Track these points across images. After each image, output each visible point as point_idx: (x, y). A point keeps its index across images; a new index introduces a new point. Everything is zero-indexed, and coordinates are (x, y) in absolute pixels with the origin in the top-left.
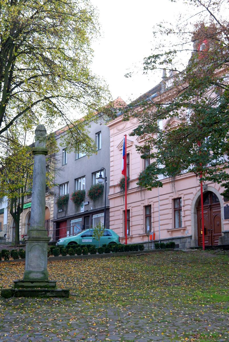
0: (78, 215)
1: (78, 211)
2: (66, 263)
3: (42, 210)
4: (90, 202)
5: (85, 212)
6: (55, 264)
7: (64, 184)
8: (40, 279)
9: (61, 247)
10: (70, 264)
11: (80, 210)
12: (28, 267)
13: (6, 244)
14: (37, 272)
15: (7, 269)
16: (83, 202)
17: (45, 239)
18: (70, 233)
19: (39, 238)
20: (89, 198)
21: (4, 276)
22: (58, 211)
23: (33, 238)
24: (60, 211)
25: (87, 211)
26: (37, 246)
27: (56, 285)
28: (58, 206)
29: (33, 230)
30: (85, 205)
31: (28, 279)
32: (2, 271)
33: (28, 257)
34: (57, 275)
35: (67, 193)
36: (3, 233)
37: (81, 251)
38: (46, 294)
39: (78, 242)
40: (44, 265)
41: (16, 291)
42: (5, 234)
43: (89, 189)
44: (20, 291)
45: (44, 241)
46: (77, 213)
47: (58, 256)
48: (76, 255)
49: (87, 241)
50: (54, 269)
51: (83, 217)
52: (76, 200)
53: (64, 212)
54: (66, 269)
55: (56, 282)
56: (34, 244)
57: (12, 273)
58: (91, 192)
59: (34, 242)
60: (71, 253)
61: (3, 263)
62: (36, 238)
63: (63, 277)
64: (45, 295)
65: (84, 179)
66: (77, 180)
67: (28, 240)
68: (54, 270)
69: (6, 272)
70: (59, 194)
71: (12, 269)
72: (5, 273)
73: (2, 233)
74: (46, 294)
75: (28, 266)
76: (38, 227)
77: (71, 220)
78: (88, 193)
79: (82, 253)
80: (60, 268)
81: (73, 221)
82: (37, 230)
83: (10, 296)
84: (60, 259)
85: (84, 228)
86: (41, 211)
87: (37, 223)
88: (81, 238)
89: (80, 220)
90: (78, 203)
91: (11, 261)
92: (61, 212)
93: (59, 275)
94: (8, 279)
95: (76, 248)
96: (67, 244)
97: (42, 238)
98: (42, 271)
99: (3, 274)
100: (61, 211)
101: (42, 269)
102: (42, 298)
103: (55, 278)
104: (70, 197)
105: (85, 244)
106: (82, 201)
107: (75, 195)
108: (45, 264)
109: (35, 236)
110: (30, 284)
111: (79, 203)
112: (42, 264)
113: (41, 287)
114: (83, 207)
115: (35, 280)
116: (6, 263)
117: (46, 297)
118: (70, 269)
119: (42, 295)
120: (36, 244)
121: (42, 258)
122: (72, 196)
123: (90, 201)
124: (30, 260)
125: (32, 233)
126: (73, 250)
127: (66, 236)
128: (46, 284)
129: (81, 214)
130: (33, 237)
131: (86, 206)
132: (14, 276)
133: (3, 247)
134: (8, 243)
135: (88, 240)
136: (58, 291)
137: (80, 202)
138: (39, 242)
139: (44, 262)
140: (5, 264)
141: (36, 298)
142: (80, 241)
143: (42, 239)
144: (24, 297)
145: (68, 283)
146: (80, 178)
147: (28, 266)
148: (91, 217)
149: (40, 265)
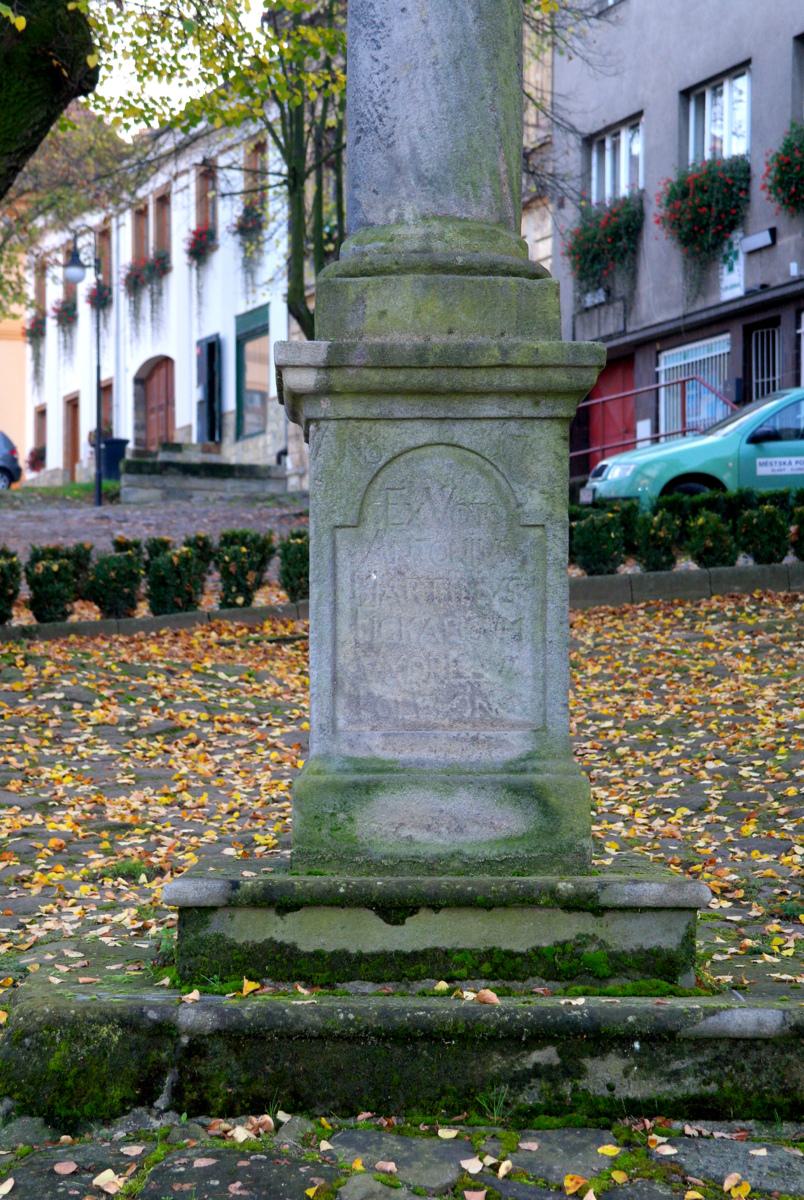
0: (704, 316)
1: (705, 295)
2: (680, 621)
3: (480, 14)
4: (781, 230)
5: (749, 293)
6: (597, 634)
7: (613, 129)
8: (488, 865)
9: (626, 511)
10: (712, 630)
11: (717, 289)
12: (341, 723)
13: (280, 504)
14: (452, 778)
15: (222, 675)
16: (737, 235)
17: (531, 379)
18: (656, 428)
19: (457, 360)
20: (776, 204)
21: (193, 745)
22: (578, 301)
23: (383, 359)
24: (590, 300)
25: (764, 287)
26: (437, 464)
27: (689, 938)
28: (582, 269)
29: (387, 261)
30: (751, 253)
31: (350, 856)
32: (178, 700)
33: (335, 604)
34: (630, 728)
35: (633, 184)
36: (269, 442)
37: (783, 532)
38: (581, 1072)
39: (727, 478)
40: (526, 691)
41: (189, 1033)
42: (280, 447)
43: (775, 143)
44: (239, 1036)
45: (518, 393)
46: (699, 306)
47: (612, 572)
48: (744, 561)
49: (788, 471)
50: (595, 677)
51: (738, 328)
52: (692, 220)
53: (619, 305)
54: (693, 671)
55: (694, 910)
56: (394, 437)
57: (258, 714)
58: (789, 164)
59: (400, 407)
60: (708, 551)
61: (213, 629)
62: (420, 359)
63: (686, 755)
64: (566, 1089)
65: (743, 83)
66: (693, 95)
67: (325, 391)
68: (594, 687)
69: (211, 708)
70: (584, 196)
71: (267, 675)
72: (204, 716)
73: (265, 447)
74: (571, 1069)
75: (342, 702)
76: (436, 227)
77: (659, 352)
78: (772, 173)
79: (794, 544)
80: (637, 664)
81: (671, 360)
82: (436, 268)
83: (116, 1093)
84: (632, 590)
85: (743, 396)
86: (474, 29)
87: (420, 178)
88: (752, 447)
89: (720, 345)
90: (701, 245)
91: (270, 612)
92: (596, 306)
93: (644, 734)
94: (219, 774)
95: (746, 513)
96: (656, 492)
97: (495, 355)
98: (510, 768)
99: (182, 728)
100: (600, 297)
101: (501, 743)
102: (523, 1120)
103: (619, 761)
104: (654, 210)
105: (782, 489)
106: (732, 226)
107: (685, 194)
108: (543, 680)
109: (404, 339)
110: (374, 936)
111: (710, 238)
112: (507, 674)
113: (501, 967)
114: (740, 265)
115: (427, 881)
116: (232, 630)
117: (579, 1116)
118: (724, 672)
119: (519, 1081)
120: (426, 433)
121: (497, 606)
122: (664, 201)
123: (781, 222)
124: (363, 637)
125: (373, 305)
126: (726, 528)
127: (630, 446)
128: (568, 927)
129: (724, 309)
130: (382, 349)
131: (755, 259)
132: (274, 747)
133: (259, 517)
134: (294, 499)
135: (793, 460)
136: (735, 1041)
137: (717, 234)
138: (460, 407)
139: (523, 659)
140: (226, 637)
141: (446, 1133)
142: (745, 466)
143: (496, 379)
144: (298, 1105)
145: (749, 829)
146: (715, 82)
147: (342, 702)
148: (793, 323)
149: (476, 690)
